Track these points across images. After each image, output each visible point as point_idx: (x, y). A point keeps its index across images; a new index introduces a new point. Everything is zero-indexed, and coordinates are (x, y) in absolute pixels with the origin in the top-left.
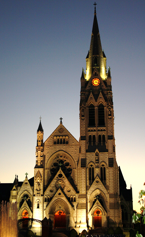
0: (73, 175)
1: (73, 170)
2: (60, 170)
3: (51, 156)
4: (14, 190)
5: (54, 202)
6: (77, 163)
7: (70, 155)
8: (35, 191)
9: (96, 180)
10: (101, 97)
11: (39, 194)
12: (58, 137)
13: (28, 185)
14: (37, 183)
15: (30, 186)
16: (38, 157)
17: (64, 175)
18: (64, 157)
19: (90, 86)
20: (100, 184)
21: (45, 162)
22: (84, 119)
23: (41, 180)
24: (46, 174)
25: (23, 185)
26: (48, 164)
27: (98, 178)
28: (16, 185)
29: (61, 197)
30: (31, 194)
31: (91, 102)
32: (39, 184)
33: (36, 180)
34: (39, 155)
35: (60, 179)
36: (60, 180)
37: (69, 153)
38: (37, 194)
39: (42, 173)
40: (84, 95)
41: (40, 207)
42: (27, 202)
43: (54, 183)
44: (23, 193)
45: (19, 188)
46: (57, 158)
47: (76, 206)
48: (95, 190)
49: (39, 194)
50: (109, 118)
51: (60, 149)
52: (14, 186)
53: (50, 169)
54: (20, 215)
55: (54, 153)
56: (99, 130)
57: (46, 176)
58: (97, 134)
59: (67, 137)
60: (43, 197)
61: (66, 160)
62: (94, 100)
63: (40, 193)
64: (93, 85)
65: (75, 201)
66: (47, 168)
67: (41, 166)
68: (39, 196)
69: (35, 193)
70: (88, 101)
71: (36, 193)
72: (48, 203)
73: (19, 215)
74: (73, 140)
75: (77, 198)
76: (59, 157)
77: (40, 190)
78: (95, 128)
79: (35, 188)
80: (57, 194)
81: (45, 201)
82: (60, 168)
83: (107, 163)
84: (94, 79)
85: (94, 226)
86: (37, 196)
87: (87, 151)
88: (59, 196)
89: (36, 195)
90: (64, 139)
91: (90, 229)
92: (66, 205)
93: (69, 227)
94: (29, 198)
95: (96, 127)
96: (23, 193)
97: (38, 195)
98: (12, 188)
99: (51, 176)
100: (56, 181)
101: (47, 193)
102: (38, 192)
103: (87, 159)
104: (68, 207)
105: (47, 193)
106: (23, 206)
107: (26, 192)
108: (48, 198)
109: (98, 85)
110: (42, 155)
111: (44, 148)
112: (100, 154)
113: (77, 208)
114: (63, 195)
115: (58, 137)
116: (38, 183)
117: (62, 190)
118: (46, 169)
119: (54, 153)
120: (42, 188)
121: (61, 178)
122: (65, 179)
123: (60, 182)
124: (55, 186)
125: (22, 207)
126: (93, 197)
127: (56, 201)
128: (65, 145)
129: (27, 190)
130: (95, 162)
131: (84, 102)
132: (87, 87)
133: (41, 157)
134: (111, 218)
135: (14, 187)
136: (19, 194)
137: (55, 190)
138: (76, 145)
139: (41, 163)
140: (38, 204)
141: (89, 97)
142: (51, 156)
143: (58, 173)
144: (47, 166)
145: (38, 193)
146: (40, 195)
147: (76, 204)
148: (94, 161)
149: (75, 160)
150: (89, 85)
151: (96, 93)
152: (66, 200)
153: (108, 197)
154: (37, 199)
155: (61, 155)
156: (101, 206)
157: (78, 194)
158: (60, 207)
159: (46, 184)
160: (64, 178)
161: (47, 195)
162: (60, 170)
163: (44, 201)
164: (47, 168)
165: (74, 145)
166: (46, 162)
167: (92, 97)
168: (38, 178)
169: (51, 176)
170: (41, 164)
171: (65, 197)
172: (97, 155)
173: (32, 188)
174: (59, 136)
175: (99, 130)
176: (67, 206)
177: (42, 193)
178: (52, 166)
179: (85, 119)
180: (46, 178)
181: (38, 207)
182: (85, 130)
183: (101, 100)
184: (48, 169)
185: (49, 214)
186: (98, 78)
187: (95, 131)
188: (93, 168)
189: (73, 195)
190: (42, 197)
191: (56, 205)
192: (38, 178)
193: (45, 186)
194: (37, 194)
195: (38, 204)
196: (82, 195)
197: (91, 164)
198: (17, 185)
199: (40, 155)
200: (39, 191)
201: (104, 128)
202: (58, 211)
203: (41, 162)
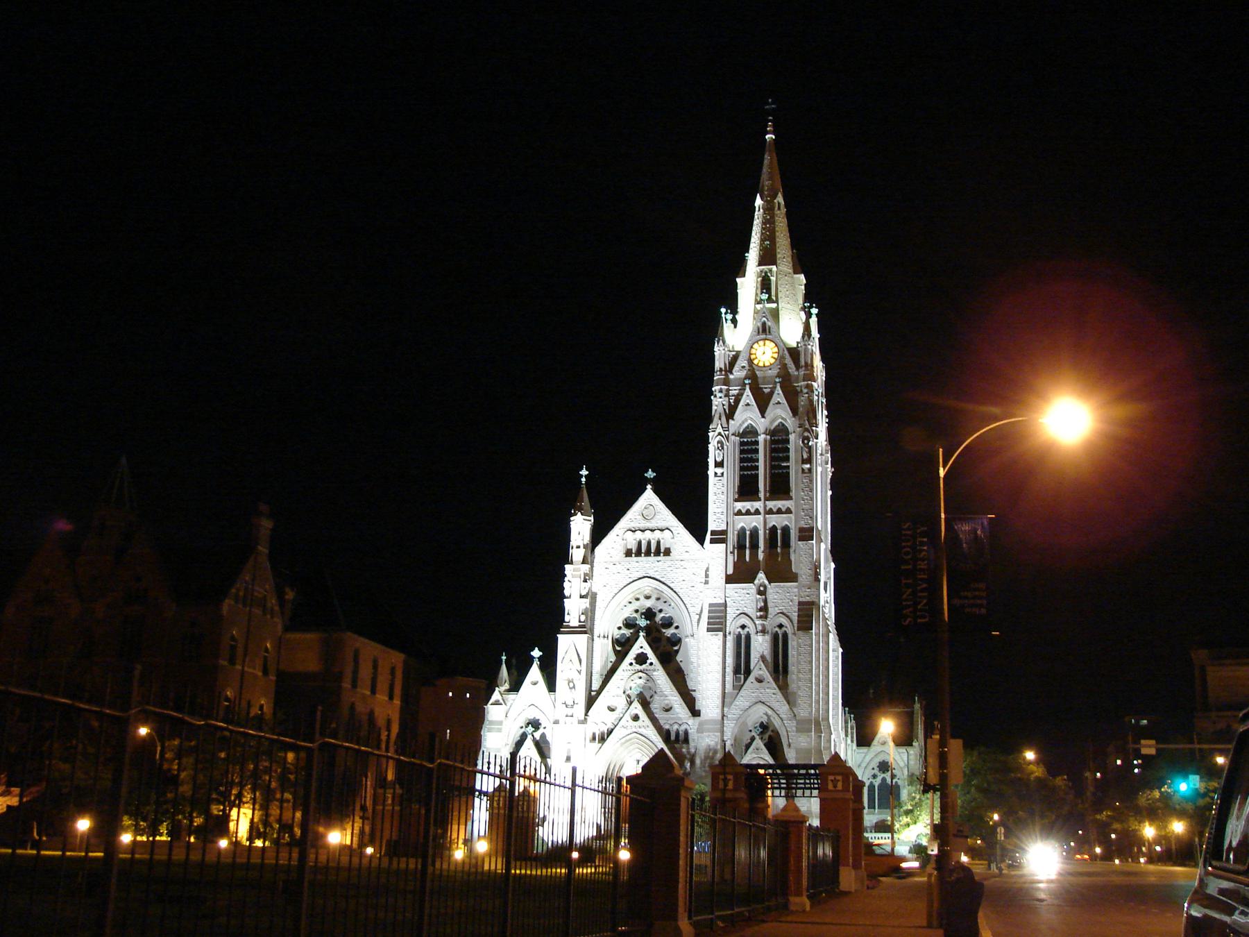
4: (497, 703)
18: (658, 599)
19: (743, 367)
20: (768, 685)
23: (579, 672)
32: (571, 685)
61: (664, 607)
67: (580, 627)
78: (758, 505)
82: (642, 634)
87: (730, 579)
102: (569, 711)
115: (639, 535)
121: (644, 666)
124: (624, 692)
132: (736, 368)
133: (581, 597)
139: (583, 618)
167: (750, 400)
172: (762, 592)
187: (757, 512)
188: (748, 637)
193: (593, 693)
198: (507, 686)
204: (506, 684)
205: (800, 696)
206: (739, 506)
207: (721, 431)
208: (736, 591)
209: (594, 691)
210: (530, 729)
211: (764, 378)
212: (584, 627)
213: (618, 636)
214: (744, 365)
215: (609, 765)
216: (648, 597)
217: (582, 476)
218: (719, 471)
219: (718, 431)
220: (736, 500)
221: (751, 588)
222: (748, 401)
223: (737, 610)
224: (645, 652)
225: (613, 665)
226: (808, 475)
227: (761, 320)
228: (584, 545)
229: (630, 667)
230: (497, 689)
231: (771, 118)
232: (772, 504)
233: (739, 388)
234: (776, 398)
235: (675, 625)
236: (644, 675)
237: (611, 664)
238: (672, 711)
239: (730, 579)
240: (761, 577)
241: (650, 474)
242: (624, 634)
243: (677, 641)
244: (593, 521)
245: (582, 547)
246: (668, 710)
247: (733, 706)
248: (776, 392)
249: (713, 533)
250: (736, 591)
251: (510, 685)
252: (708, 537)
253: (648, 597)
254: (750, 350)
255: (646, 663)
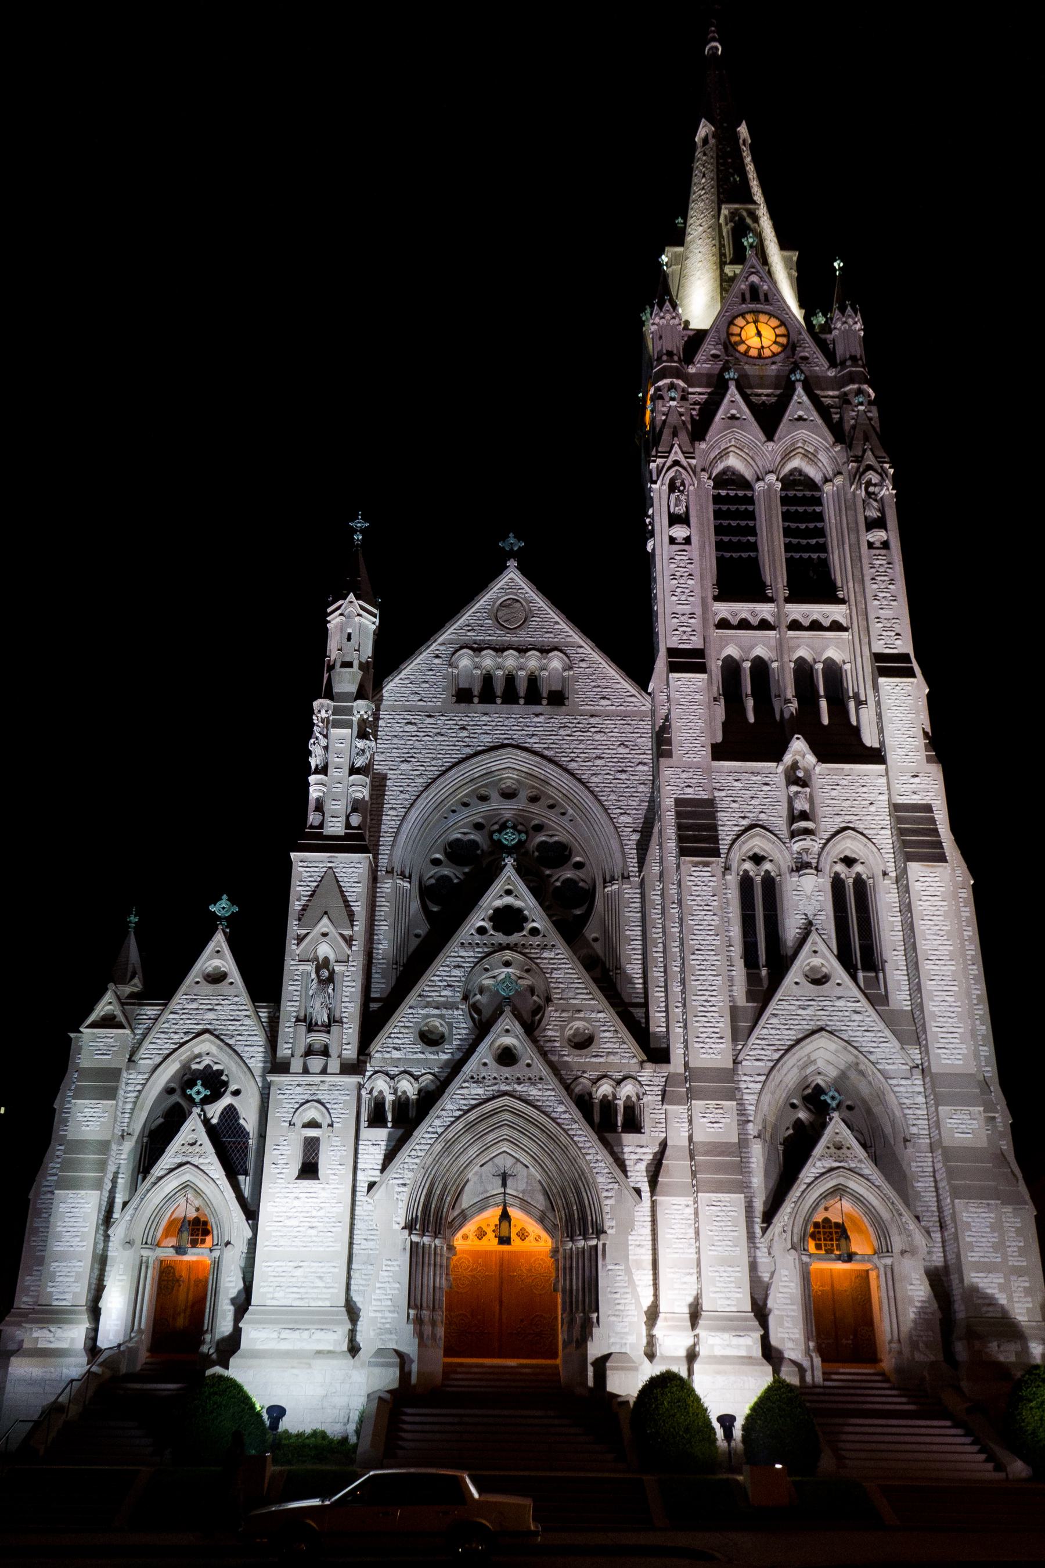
0: (605, 931)
1: (606, 897)
2: (509, 873)
3: (435, 780)
4: (108, 1022)
5: (460, 1125)
6: (636, 837)
7: (580, 780)
8: (287, 1028)
9: (804, 961)
10: (800, 418)
11: (325, 1052)
12: (488, 660)
13: (231, 991)
14: (310, 968)
15: (244, 998)
16: (330, 770)
17: (538, 919)
18: (534, 799)
19: (715, 356)
20: (839, 992)
21: (379, 823)
22: (688, 540)
23: (349, 941)
24: (385, 907)
25: (183, 988)
26: (402, 838)
27: (822, 947)
28: (128, 990)
29: (519, 1081)
30: (252, 1063)
31: (724, 454)
32: (325, 973)
33: (300, 939)
34: (334, 760)
35: (508, 947)
36: (508, 955)
37: (572, 766)
38: (309, 1052)
39: (356, 890)
40: (684, 398)
41: (322, 1171)
42: (212, 1131)
43: (456, 972)
44: (184, 1053)
45: (151, 1011)
46: (474, 801)
47: (642, 1166)
48: (799, 1041)
49: (325, 1052)
50: (870, 545)
51: (500, 737)
52: (104, 990)
53: (415, 879)
54: (138, 1236)
55: (455, 765)
56: (795, 625)
57: (384, 929)
58: (781, 647)
59: (556, 662)
60: (360, 1086)
61: (551, 819)
62: (752, 432)
63: (333, 1051)
64: (742, 348)
65: (633, 1124)
66: (398, 868)
67: (347, 837)
68: (324, 1071)
69: (284, 1051)
70: (710, 434)
71: (301, 1050)
72: (400, 1132)
73: (130, 1243)
74: (604, 683)
75: (651, 1099)
76: (495, 795)
77: (333, 1021)
78: (765, 610)
79: (290, 1007)
80: (484, 1052)
81: (377, 1119)
82: (509, 861)
83: (886, 838)
84: (743, 315)
85: (820, 1350)
86: (306, 1071)
87: (719, 752)
88: (506, 1072)
89: (296, 1065)
90: (533, 680)
91: (241, 1178)
92: (564, 1150)
93: (595, 1350)
94: (226, 1100)
95: (770, 600)
96: (184, 1053)
97: (316, 1063)
98: (91, 1010)
99: (429, 934)
100: (469, 955)
101: (396, 1054)
102: (319, 1038)
103: (721, 805)
104: (582, 1174)
105: (396, 1054)
106: (168, 1160)
107: (206, 1045)
108: (402, 1105)
109: (774, 355)
110: (360, 762)
111: (376, 717)
112: (822, 772)
113: (653, 1182)
114: (540, 1068)
115: (488, 660)
116: (323, 964)
117: (531, 1028)
118: (390, 872)
119: (455, 765)
120: (350, 1008)
121: (515, 938)
122: (545, 947)
123: (507, 964)
124: (465, 998)
125: (157, 1170)
126: (782, 1095)
127: (472, 1116)
128: (538, 709)
129: (221, 1029)
130: (785, 834)
131: (684, 437)
132: (700, 357)
133: (353, 771)
134: (975, 1278)
135: (109, 996)
136: (150, 1052)
137: (461, 1028)
138: (623, 716)
139: (355, 820)
140: (311, 1146)
141: (720, 414)
142: (427, 786)
143: (493, 900)
144: (399, 851)
145: (317, 1046)
146: (334, 1065)
147: (648, 1153)
148: (779, 821)
149: (624, 819)
150: (709, 347)
151: (765, 394)
152: (566, 1112)
153: (921, 1099)
154: (300, 1094)
155: (510, 779)
156: (868, 1168)
157: (665, 1070)
158: (504, 1178)
159: (380, 987)
160: (536, 941)
161: (394, 1071)
162: (509, 873)
163: (364, 1116)
164: (398, 868)
165: (608, 715)
166: (389, 822)
167: (739, 410)
168: (325, 925)
169: (423, 929)
170: (348, 826)
171: (552, 1082)
172: (795, 778)
173: (264, 1015)
174: (500, 649)
175: (795, 625)
176: (573, 1161)
177: (350, 1052)
178: (436, 862)
179: (694, 540)
180: (384, 946)
181: (309, 1170)
182: (698, 611)
183: (802, 433)
184: (402, 875)
185: (410, 1227)
186: (771, 315)
187: (764, 625)
188: (770, 884)
189: (618, 1076)
190: (353, 1080)
191: (472, 1151)
192: (325, 925)
193: (374, 1006)
194: (309, 1052)
195: (311, 1146)
196: (691, 1073)
197: (757, 843)
198: (136, 985)
199: (344, 761)
200: (327, 1028)
201: (836, 612)
202: (482, 1205)
203: (354, 810)
204: (136, 981)
205: (934, 1016)
206: (724, 610)
207: (680, 457)
208: (737, 776)
209: (376, 1000)
210: (199, 1091)
211: (761, 377)
212: (360, 836)
213: (433, 881)
214: (718, 352)
215: (432, 1185)
216: (509, 795)
217: (354, 531)
218: (680, 532)
219: (672, 457)
220: (716, 599)
221: (776, 770)
222: (734, 412)
223: (744, 818)
224: (518, 904)
225: (422, 942)
226: (883, 552)
227: (747, 278)
228: (360, 663)
229: (477, 938)
230: (111, 986)
231: (713, 29)
232: (797, 611)
233: (709, 390)
234: (794, 410)
235: (233, 1087)
236: (517, 955)
237: (418, 941)
238: (593, 1049)
239: (719, 752)
240: (798, 748)
241: (513, 543)
242: (447, 877)
243: (500, 944)
244: (377, 624)
245: (356, 664)
246: (583, 1042)
247: (752, 1039)
248: (795, 397)
249: (672, 652)
250: (737, 776)
251: (145, 982)
252: (661, 663)
253: (509, 795)
254: (728, 327)
255: (522, 929)
